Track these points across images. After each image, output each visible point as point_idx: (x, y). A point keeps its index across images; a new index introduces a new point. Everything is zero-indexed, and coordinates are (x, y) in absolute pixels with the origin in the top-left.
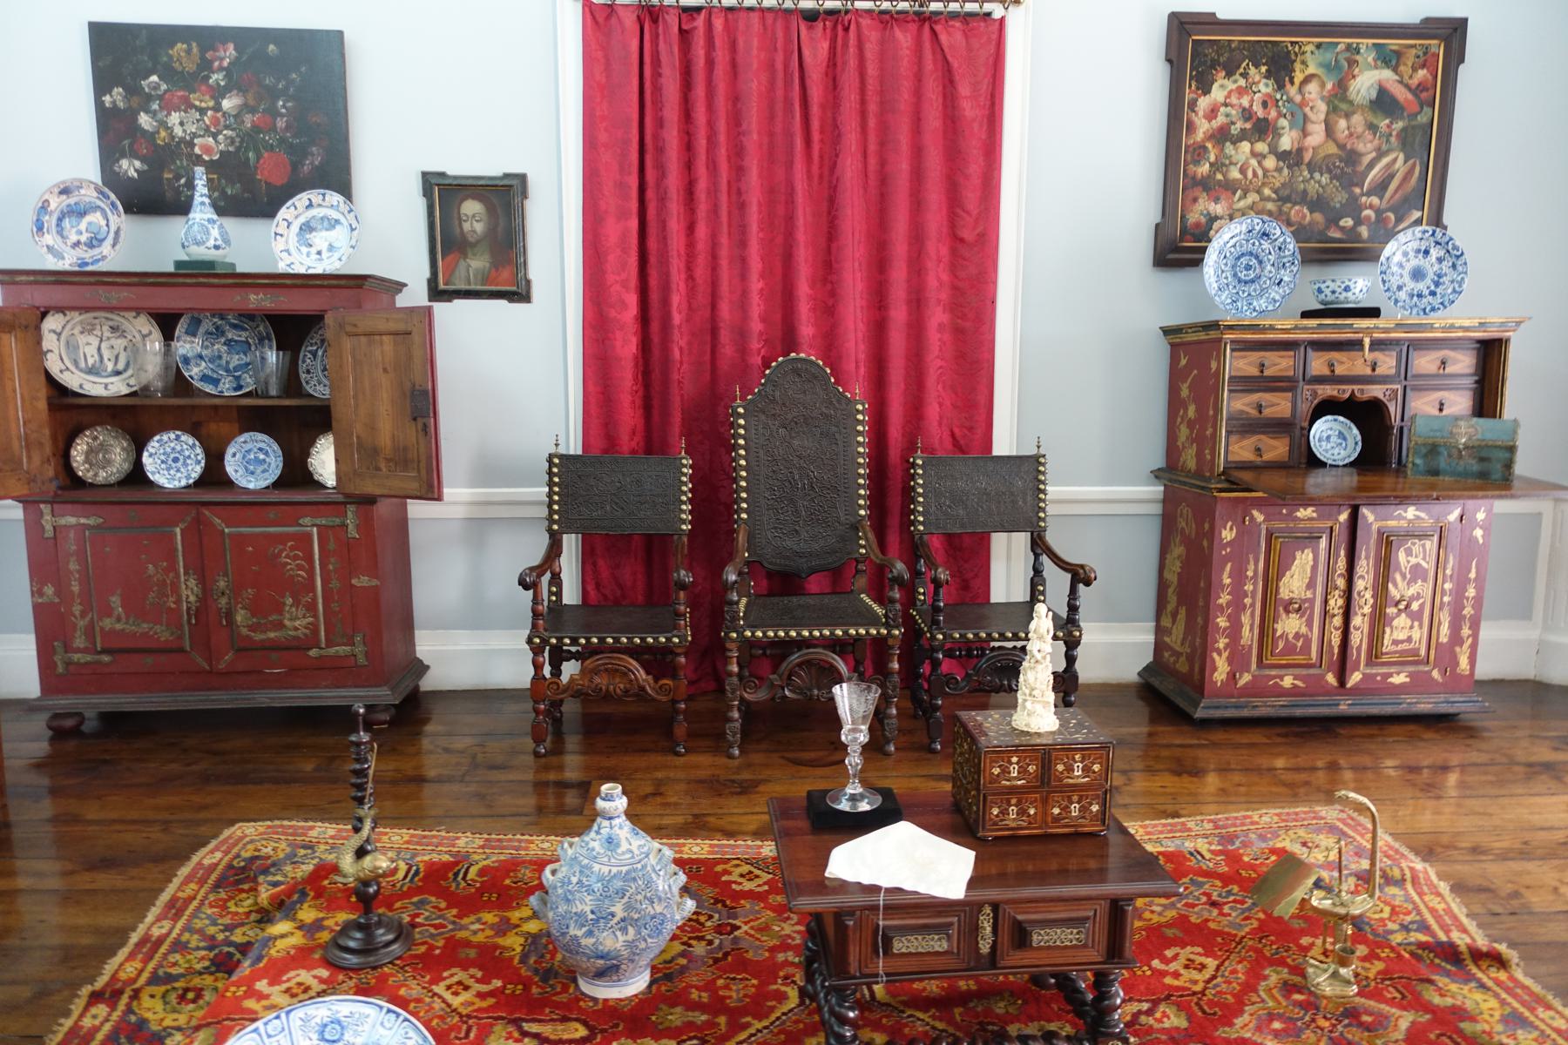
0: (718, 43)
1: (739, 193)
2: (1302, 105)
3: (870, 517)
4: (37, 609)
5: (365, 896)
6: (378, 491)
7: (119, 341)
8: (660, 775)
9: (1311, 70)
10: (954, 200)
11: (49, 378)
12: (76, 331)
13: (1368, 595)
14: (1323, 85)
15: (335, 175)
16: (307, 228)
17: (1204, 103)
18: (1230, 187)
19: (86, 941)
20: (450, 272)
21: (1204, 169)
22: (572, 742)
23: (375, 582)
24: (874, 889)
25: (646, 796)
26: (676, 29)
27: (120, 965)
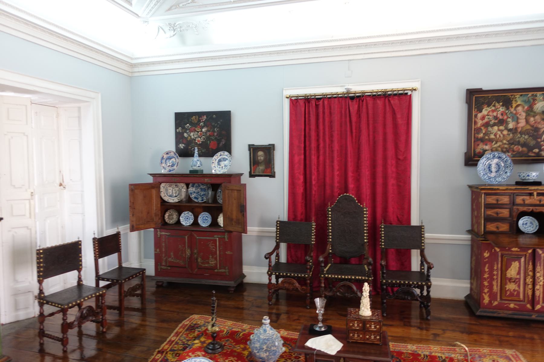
0: (326, 107)
1: (332, 147)
2: (516, 114)
3: (368, 242)
4: (156, 255)
5: (215, 336)
6: (232, 230)
8: (301, 314)
9: (519, 103)
10: (396, 147)
11: (161, 198)
13: (542, 278)
14: (524, 107)
15: (228, 148)
16: (220, 161)
17: (480, 115)
18: (491, 141)
19: (158, 339)
20: (254, 170)
21: (481, 135)
22: (283, 301)
23: (231, 253)
24: (315, 350)
25: (295, 320)
26: (314, 105)
27: (164, 346)
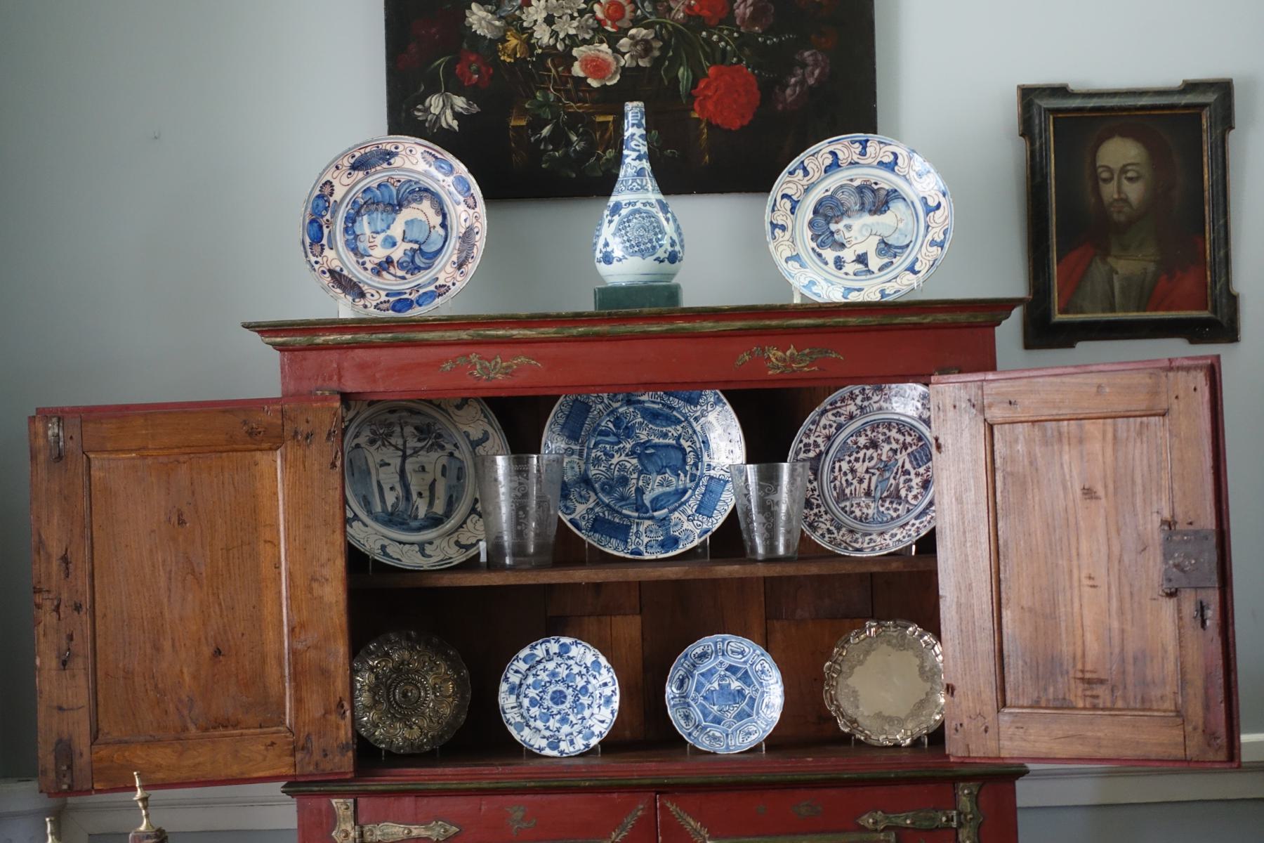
7: (434, 455)
12: (362, 440)
